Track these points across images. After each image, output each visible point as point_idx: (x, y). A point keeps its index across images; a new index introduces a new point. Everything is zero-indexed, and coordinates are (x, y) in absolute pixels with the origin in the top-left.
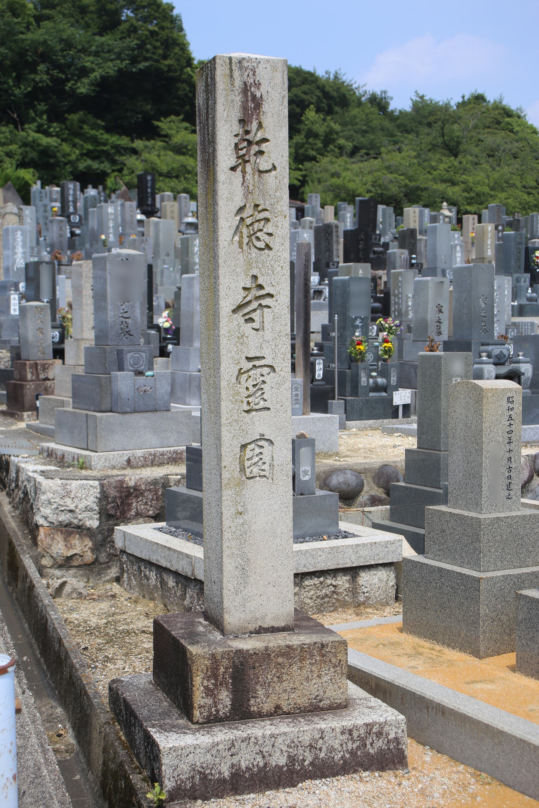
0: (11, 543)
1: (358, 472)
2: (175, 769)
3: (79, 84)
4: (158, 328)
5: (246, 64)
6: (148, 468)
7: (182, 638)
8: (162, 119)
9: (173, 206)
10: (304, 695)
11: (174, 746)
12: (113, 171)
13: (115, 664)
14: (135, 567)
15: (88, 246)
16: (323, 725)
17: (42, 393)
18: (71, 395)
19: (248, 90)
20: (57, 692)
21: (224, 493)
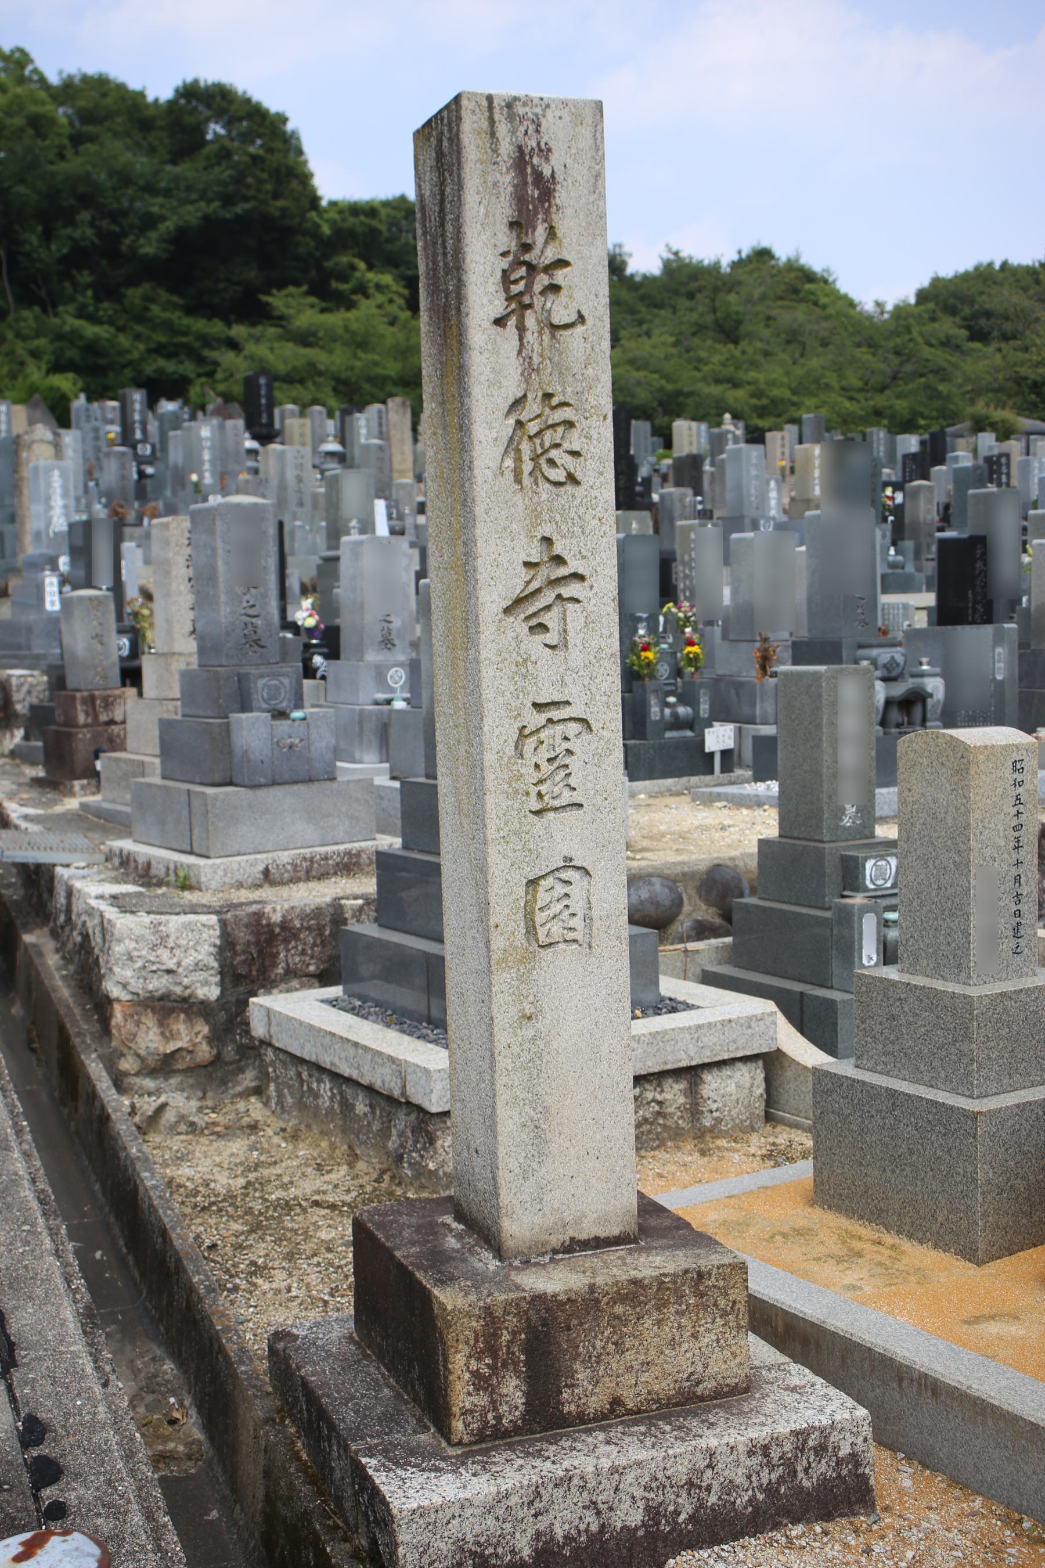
0: (62, 1029)
1: (673, 880)
2: (425, 1552)
3: (142, 241)
4: (295, 628)
5: (520, 110)
6: (301, 885)
7: (418, 1269)
8: (274, 291)
9: (303, 425)
10: (666, 1375)
11: (420, 1507)
12: (199, 375)
13: (270, 1278)
14: (292, 1073)
15: (168, 493)
16: (711, 1440)
17: (105, 746)
18: (158, 751)
19: (526, 163)
20: (162, 1328)
21: (495, 978)
